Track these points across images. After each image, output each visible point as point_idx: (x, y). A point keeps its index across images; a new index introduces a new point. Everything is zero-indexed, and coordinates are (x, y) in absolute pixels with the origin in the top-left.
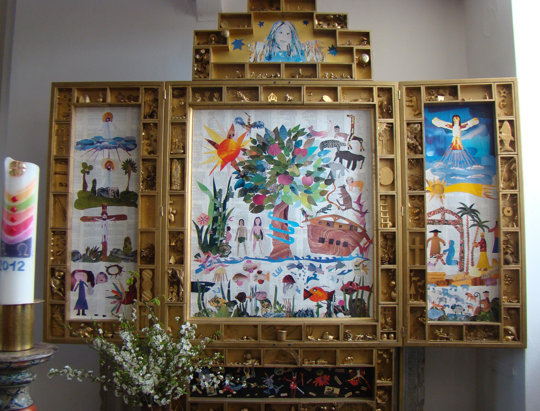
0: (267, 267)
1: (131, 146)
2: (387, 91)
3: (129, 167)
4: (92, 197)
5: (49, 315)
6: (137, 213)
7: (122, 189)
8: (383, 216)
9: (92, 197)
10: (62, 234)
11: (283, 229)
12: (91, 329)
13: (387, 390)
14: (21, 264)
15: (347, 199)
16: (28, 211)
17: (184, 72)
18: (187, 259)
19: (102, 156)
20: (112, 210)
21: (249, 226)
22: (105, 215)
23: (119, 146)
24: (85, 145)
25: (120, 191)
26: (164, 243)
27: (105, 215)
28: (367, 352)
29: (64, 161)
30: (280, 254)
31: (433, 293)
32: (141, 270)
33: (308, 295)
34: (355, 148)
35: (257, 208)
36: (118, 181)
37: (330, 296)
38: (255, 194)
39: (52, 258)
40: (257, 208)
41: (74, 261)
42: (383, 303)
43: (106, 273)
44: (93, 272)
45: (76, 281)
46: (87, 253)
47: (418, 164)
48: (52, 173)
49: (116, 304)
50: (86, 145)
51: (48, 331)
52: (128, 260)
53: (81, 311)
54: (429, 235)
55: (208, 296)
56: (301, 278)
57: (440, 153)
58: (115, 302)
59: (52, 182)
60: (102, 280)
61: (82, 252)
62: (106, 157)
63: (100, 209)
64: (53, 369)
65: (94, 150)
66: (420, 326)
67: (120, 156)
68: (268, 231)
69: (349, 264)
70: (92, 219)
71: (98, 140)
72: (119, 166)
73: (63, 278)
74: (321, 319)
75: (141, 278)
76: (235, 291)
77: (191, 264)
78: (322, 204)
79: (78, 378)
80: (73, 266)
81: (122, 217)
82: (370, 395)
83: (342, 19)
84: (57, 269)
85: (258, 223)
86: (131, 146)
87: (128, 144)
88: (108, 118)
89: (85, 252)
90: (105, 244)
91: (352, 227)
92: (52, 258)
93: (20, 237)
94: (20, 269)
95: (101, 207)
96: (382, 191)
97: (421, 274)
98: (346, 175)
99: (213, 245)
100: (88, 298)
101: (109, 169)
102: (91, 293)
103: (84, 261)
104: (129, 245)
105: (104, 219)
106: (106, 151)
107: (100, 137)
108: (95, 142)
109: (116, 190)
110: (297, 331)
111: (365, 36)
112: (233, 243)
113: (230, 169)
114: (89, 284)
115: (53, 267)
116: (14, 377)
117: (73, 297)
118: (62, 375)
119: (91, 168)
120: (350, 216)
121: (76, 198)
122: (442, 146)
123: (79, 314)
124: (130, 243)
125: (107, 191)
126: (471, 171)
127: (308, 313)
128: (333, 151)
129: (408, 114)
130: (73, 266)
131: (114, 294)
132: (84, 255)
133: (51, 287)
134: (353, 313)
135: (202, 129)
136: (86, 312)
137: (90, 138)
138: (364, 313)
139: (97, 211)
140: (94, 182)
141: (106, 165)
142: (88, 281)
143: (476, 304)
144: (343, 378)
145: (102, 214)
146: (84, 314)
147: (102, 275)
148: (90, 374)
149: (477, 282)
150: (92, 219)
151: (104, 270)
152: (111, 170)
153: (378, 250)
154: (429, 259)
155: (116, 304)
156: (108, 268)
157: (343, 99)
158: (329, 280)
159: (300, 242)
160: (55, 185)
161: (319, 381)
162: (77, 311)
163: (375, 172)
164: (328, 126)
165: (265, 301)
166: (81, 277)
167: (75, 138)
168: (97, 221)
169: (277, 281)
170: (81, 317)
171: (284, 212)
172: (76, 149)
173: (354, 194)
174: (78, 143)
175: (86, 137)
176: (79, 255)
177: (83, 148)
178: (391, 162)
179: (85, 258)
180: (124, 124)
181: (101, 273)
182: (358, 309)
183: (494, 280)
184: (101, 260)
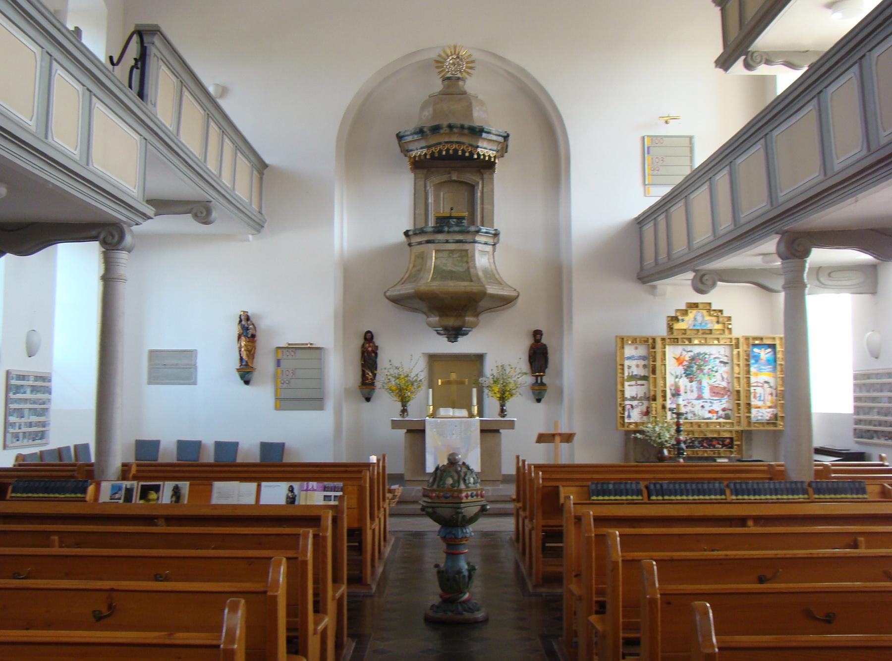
2: (737, 339)
3: (645, 366)
6: (649, 384)
8: (736, 384)
11: (700, 389)
15: (723, 378)
17: (663, 331)
18: (121, 525)
20: (639, 382)
21: (688, 388)
24: (629, 358)
28: (731, 431)
30: (700, 397)
31: (754, 411)
33: (710, 412)
34: (725, 359)
35: (691, 381)
36: (641, 372)
37: (717, 412)
38: (689, 375)
40: (691, 381)
47: (748, 366)
54: (752, 391)
56: (707, 405)
57: (757, 361)
66: (749, 423)
68: (695, 390)
69: (724, 401)
72: (641, 367)
83: (721, 311)
85: (691, 387)
88: (636, 348)
91: (725, 388)
96: (736, 375)
97: (749, 404)
98: (723, 369)
110: (707, 424)
111: (729, 318)
120: (724, 384)
122: (757, 358)
126: (769, 368)
127: (709, 418)
128: (718, 361)
129: (745, 348)
135: (672, 352)
139: (633, 383)
143: (769, 415)
153: (735, 396)
154: (752, 399)
157: (722, 343)
159: (706, 393)
161: (714, 443)
163: (732, 368)
164: (716, 352)
171: (700, 382)
173: (725, 376)
178: (738, 365)
179: (630, 400)
180: (642, 351)
182: (727, 417)
183: (774, 407)
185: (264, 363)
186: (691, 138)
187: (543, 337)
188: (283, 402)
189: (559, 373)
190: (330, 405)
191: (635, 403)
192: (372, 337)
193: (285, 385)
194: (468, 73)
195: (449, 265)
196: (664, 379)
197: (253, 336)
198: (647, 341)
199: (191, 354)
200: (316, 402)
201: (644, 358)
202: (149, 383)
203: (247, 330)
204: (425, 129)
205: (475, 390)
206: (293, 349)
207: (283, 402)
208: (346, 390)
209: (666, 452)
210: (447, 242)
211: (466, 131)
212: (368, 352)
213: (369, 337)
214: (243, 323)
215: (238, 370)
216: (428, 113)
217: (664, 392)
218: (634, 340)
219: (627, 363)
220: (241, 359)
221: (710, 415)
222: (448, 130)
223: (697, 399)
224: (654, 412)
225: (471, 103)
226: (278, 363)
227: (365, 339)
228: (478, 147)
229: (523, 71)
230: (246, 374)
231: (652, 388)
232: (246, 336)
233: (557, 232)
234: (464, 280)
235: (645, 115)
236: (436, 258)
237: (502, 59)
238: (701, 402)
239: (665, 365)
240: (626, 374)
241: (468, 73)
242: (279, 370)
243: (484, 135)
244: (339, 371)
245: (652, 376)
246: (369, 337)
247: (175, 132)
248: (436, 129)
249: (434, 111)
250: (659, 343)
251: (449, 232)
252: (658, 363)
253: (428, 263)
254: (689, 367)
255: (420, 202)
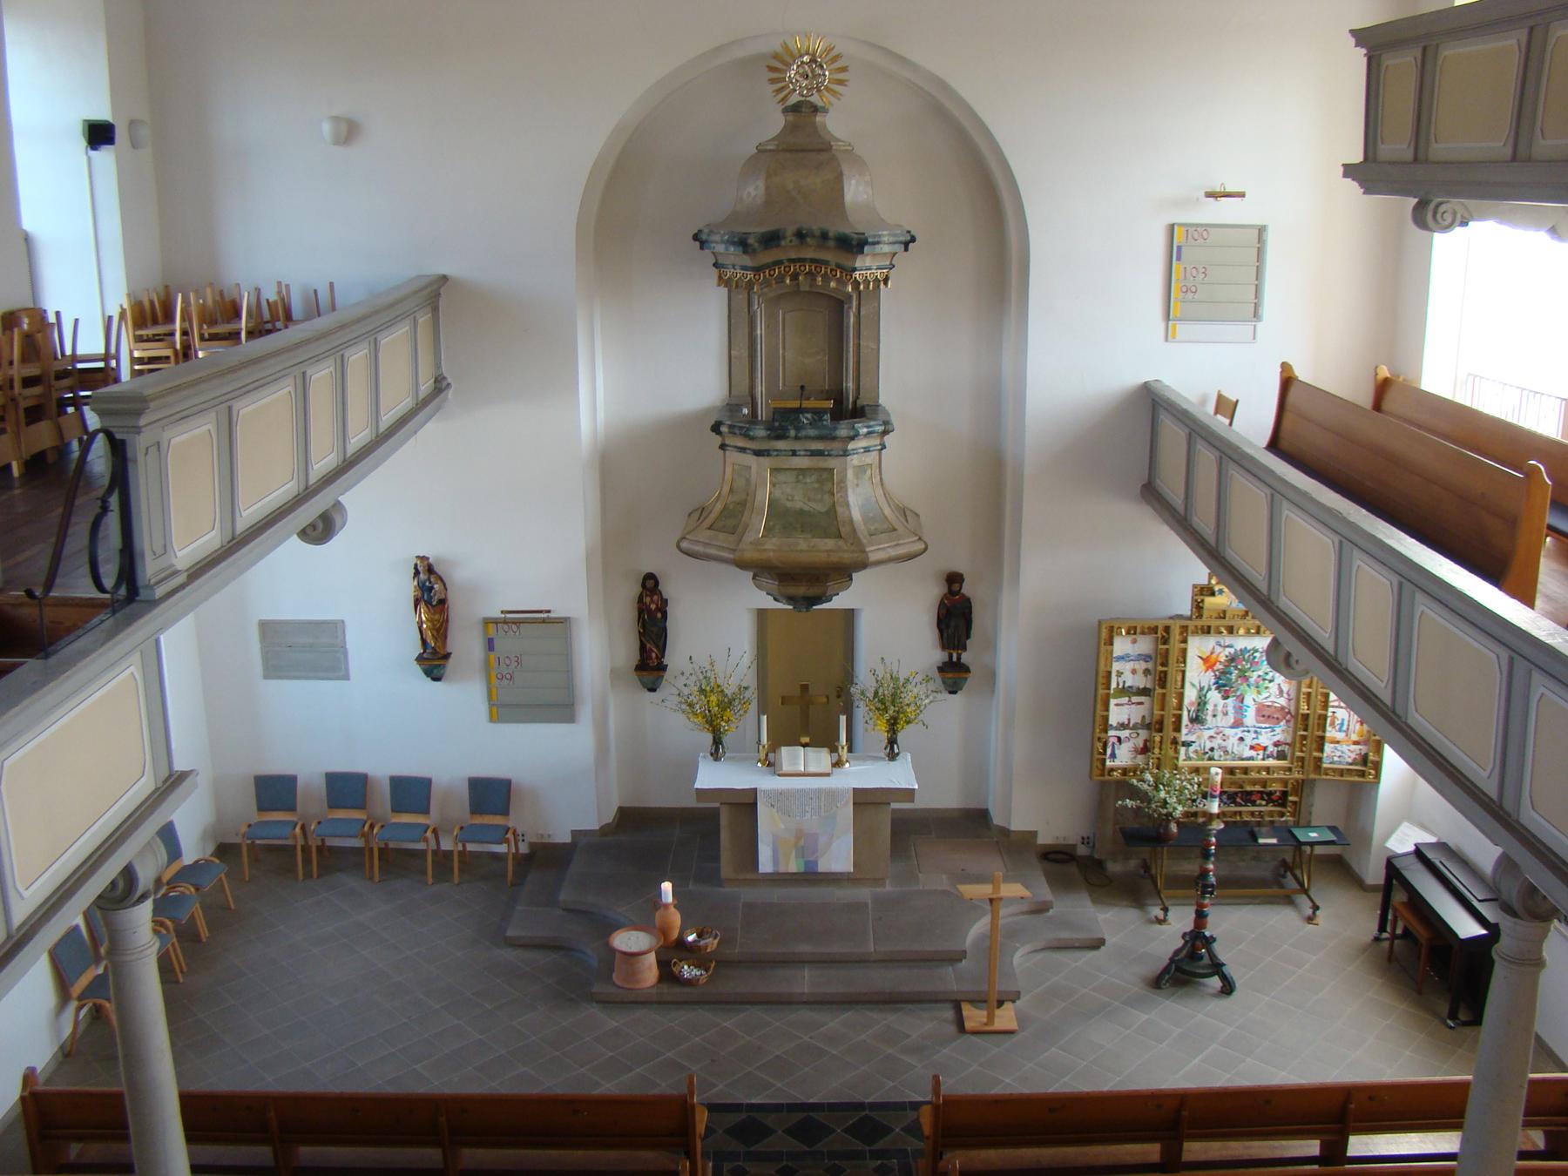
0: (1228, 732)
3: (1146, 672)
11: (1240, 710)
13: (1294, 803)
15: (1281, 692)
17: (1185, 608)
19: (1129, 666)
20: (1135, 699)
21: (1220, 708)
24: (1120, 658)
26: (1169, 722)
30: (1238, 724)
31: (1328, 748)
33: (1252, 748)
35: (1225, 697)
36: (1140, 682)
37: (1265, 748)
38: (1224, 687)
40: (1225, 697)
42: (1298, 754)
55: (1191, 749)
56: (1249, 741)
71: (1128, 655)
72: (1140, 672)
74: (1258, 763)
76: (1209, 745)
77: (1184, 731)
78: (1265, 694)
82: (1284, 805)
85: (1225, 706)
87: (1146, 658)
88: (1134, 641)
91: (1282, 708)
99: (1197, 720)
110: (1245, 770)
112: (1209, 718)
113: (1210, 674)
120: (1282, 701)
127: (1251, 758)
134: (1278, 758)
135: (1198, 647)
138: (1284, 758)
144: (1269, 797)
149: (1355, 743)
158: (1266, 739)
159: (1250, 718)
165: (1226, 752)
169: (1234, 740)
179: (1116, 729)
180: (1145, 645)
182: (1281, 756)
183: (1366, 743)
185: (465, 643)
186: (1261, 230)
187: (965, 585)
188: (501, 710)
189: (991, 645)
190: (586, 713)
191: (1124, 734)
192: (657, 583)
193: (505, 682)
194: (834, 93)
195: (797, 498)
196: (1181, 696)
197: (442, 602)
198: (1154, 630)
199: (334, 629)
200: (562, 708)
201: (1146, 658)
202: (266, 677)
203: (431, 590)
204: (751, 241)
205: (843, 719)
206: (513, 621)
207: (501, 710)
208: (614, 672)
209: (1174, 828)
210: (794, 453)
211: (831, 243)
212: (649, 610)
213: (650, 584)
214: (422, 576)
215: (420, 659)
216: (754, 191)
217: (1179, 718)
218: (1132, 631)
219: (1116, 666)
220: (424, 642)
221: (1253, 753)
222: (796, 241)
223: (1232, 727)
224: (1157, 751)
225: (841, 174)
226: (490, 645)
227: (644, 585)
228: (855, 270)
229: (944, 86)
230: (434, 661)
231: (1157, 712)
232: (428, 603)
233: (996, 398)
234: (827, 536)
235: (1200, 227)
236: (773, 485)
237: (902, 60)
238: (1239, 732)
239: (1183, 672)
240: (1114, 685)
241: (834, 93)
242: (492, 656)
243: (866, 249)
244: (598, 650)
245: (1159, 691)
246: (650, 584)
247: (185, 553)
248: (771, 239)
249: (767, 188)
250: (1176, 635)
251: (797, 438)
252: (1172, 669)
253: (758, 498)
254: (1224, 673)
255: (740, 331)
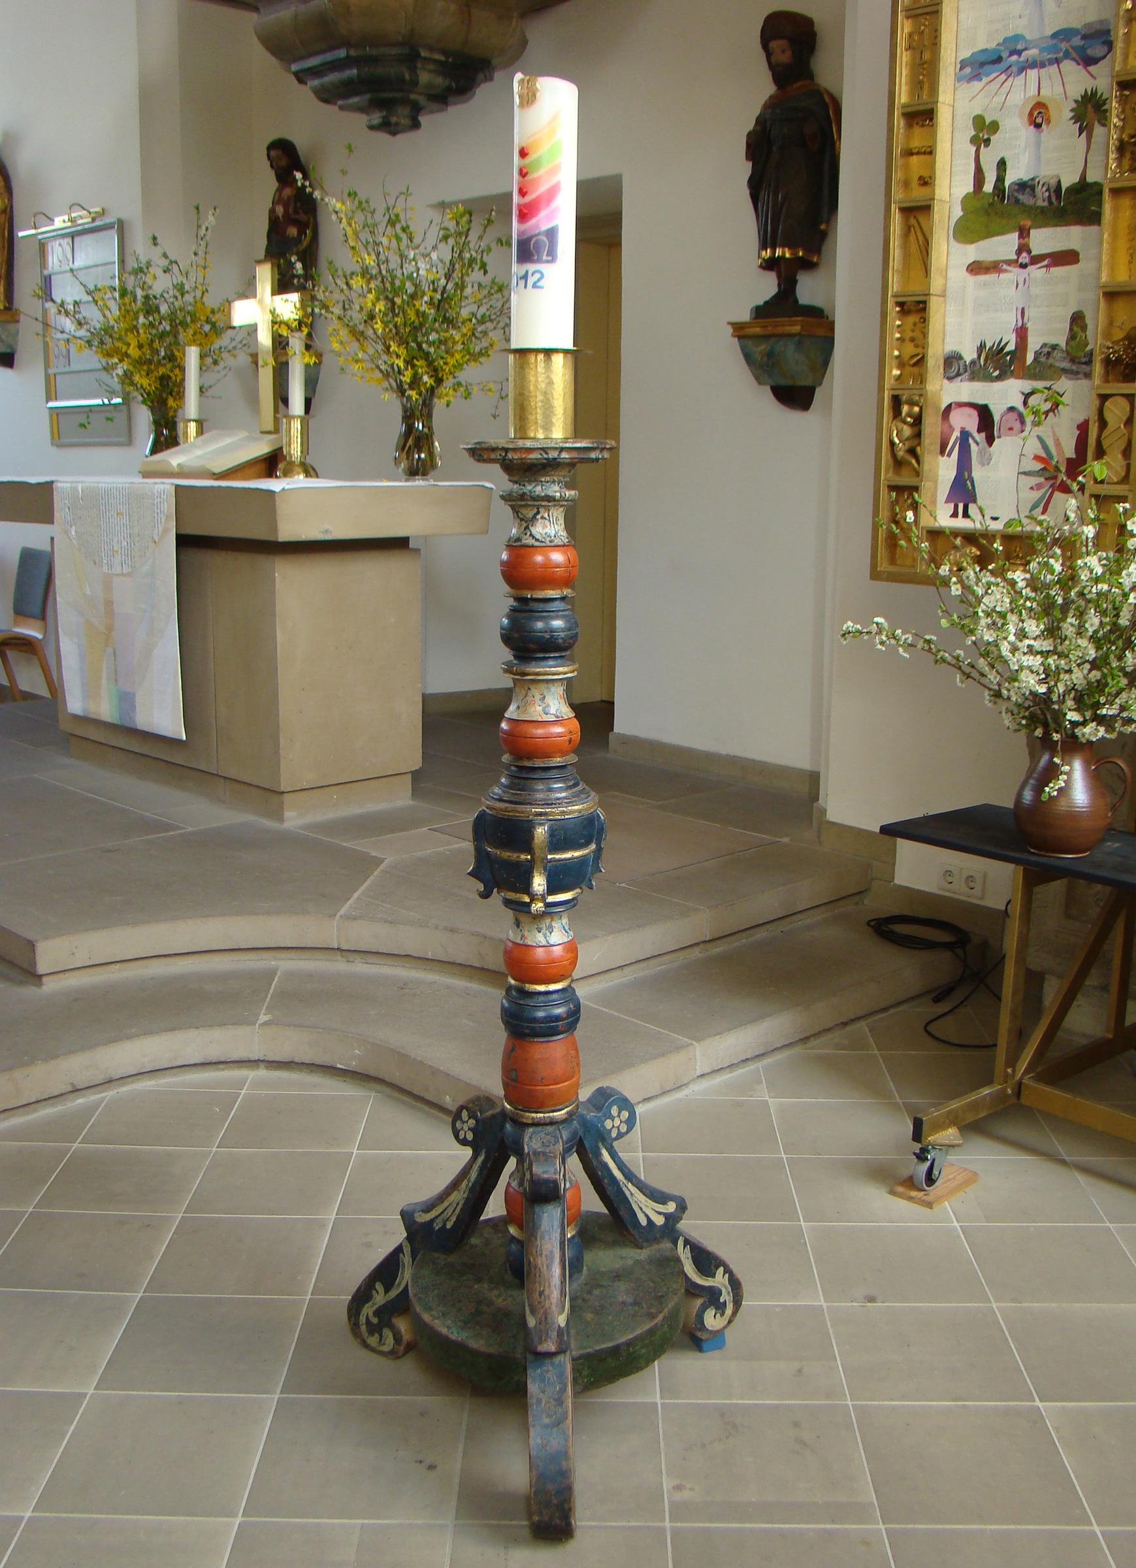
1: (1097, 50)
4: (1001, 206)
5: (884, 514)
7: (1069, 180)
9: (1001, 206)
10: (915, 308)
12: (975, 551)
14: (537, 276)
16: (554, 170)
19: (1021, 91)
20: (1044, 239)
22: (1024, 254)
23: (1067, 56)
24: (984, 64)
25: (1065, 185)
27: (1024, 254)
29: (922, 116)
32: (1104, 398)
39: (896, 372)
41: (950, 379)
43: (1021, 407)
44: (991, 407)
45: (952, 430)
46: (979, 357)
48: (897, 151)
49: (1043, 491)
50: (982, 65)
51: (882, 552)
52: (1077, 373)
53: (961, 506)
58: (1039, 486)
59: (898, 175)
60: (1011, 429)
61: (969, 355)
62: (1033, 91)
63: (1013, 239)
64: (850, 623)
65: (1003, 77)
67: (1066, 84)
70: (993, 267)
72: (1062, 114)
73: (918, 421)
75: (1103, 424)
79: (901, 650)
80: (947, 391)
81: (1067, 258)
84: (904, 398)
86: (1097, 50)
89: (975, 356)
90: (1022, 333)
92: (896, 372)
93: (541, 222)
94: (535, 286)
95: (1017, 234)
100: (978, 473)
101: (1038, 126)
102: (986, 461)
103: (972, 378)
104: (1080, 334)
105: (1023, 266)
106: (1032, 74)
107: (1017, 38)
108: (1005, 55)
109: (1053, 182)
114: (981, 437)
115: (896, 393)
116: (529, 488)
117: (944, 470)
118: (866, 637)
119: (994, 127)
121: (958, 213)
123: (955, 515)
124: (1084, 328)
125: (1033, 188)
130: (947, 391)
131: (1039, 466)
132: (973, 362)
133: (892, 444)
136: (972, 509)
137: (992, 45)
139: (1004, 245)
140: (1002, 165)
141: (1031, 114)
142: (979, 431)
145: (1019, 252)
146: (966, 515)
147: (1013, 416)
148: (929, 642)
150: (993, 267)
151: (1018, 403)
152: (1044, 126)
155: (1043, 491)
156: (1027, 396)
160: (906, 184)
162: (952, 505)
166: (966, 420)
167: (953, 49)
168: (1006, 271)
170: (961, 523)
172: (959, 79)
174: (963, 64)
175: (985, 41)
176: (961, 363)
177: (976, 77)
179: (976, 372)
181: (1012, 409)
184: (1013, 375)
